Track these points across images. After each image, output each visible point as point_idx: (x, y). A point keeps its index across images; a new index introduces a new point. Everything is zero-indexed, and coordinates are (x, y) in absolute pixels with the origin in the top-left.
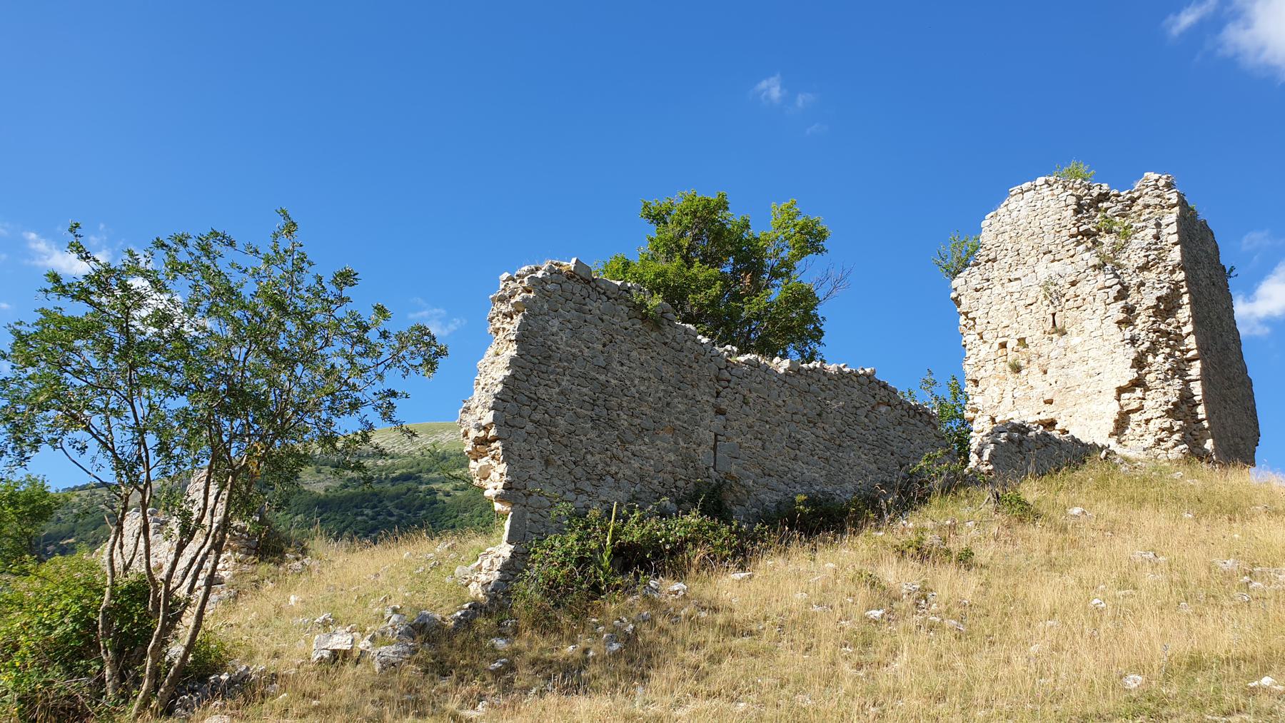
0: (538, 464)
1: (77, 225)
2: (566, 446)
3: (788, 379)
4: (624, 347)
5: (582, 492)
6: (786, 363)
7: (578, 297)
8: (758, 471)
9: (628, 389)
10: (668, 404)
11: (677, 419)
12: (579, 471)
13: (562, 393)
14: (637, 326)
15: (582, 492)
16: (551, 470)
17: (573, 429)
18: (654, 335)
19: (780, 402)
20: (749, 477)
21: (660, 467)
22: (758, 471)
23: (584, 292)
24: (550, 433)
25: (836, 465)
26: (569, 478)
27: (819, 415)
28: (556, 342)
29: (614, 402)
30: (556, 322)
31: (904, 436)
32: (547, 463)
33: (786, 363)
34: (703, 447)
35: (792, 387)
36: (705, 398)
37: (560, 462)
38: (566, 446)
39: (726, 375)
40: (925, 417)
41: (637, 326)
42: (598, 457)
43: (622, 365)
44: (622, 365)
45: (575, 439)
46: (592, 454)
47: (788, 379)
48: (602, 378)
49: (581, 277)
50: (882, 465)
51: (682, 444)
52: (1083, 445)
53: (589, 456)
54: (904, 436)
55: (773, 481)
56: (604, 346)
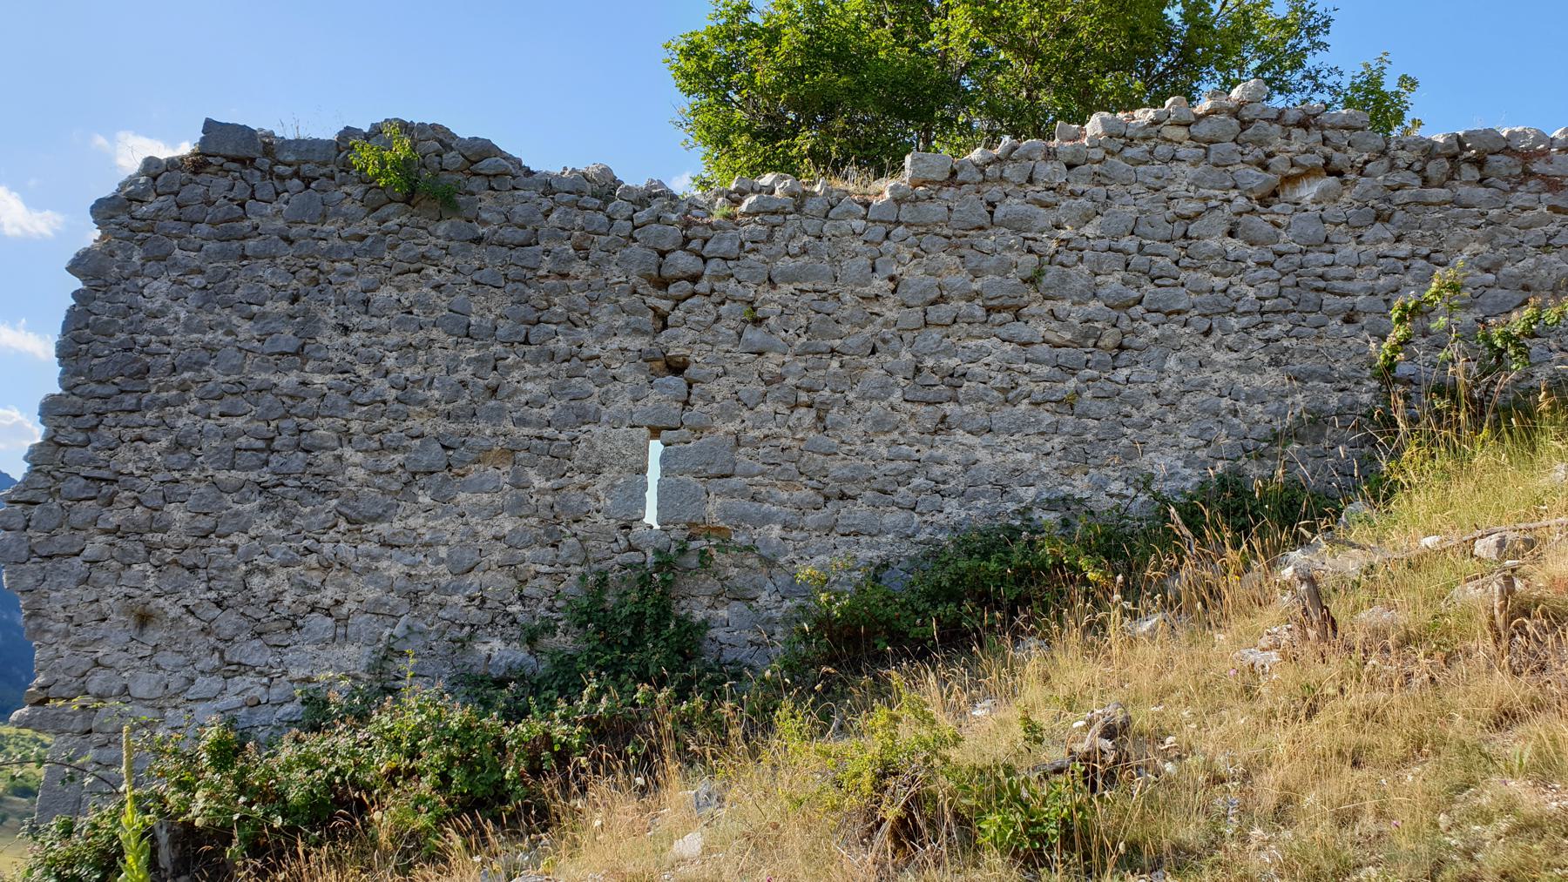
0: (119, 628)
1: (1414, 84)
2: (193, 569)
3: (906, 213)
4: (355, 285)
5: (242, 668)
6: (1177, 19)
7: (222, 207)
8: (807, 494)
9: (365, 385)
10: (494, 391)
11: (521, 422)
12: (227, 622)
13: (178, 445)
14: (392, 224)
15: (242, 668)
16: (154, 635)
17: (206, 523)
18: (443, 227)
19: (879, 284)
20: (767, 519)
21: (468, 557)
22: (807, 494)
23: (240, 190)
24: (150, 549)
25: (1105, 408)
26: (201, 644)
27: (1031, 281)
28: (160, 331)
29: (323, 430)
30: (162, 285)
31: (1404, 248)
32: (144, 620)
33: (1177, 19)
34: (608, 474)
35: (924, 228)
36: (614, 343)
37: (175, 611)
38: (193, 569)
39: (682, 261)
40: (1499, 162)
41: (392, 224)
42: (281, 574)
43: (346, 330)
44: (346, 330)
45: (217, 547)
46: (267, 572)
47: (906, 213)
48: (290, 380)
49: (233, 155)
50: (1298, 365)
51: (538, 482)
52: (548, 186)
53: (256, 581)
54: (1404, 248)
55: (859, 512)
56: (294, 299)
